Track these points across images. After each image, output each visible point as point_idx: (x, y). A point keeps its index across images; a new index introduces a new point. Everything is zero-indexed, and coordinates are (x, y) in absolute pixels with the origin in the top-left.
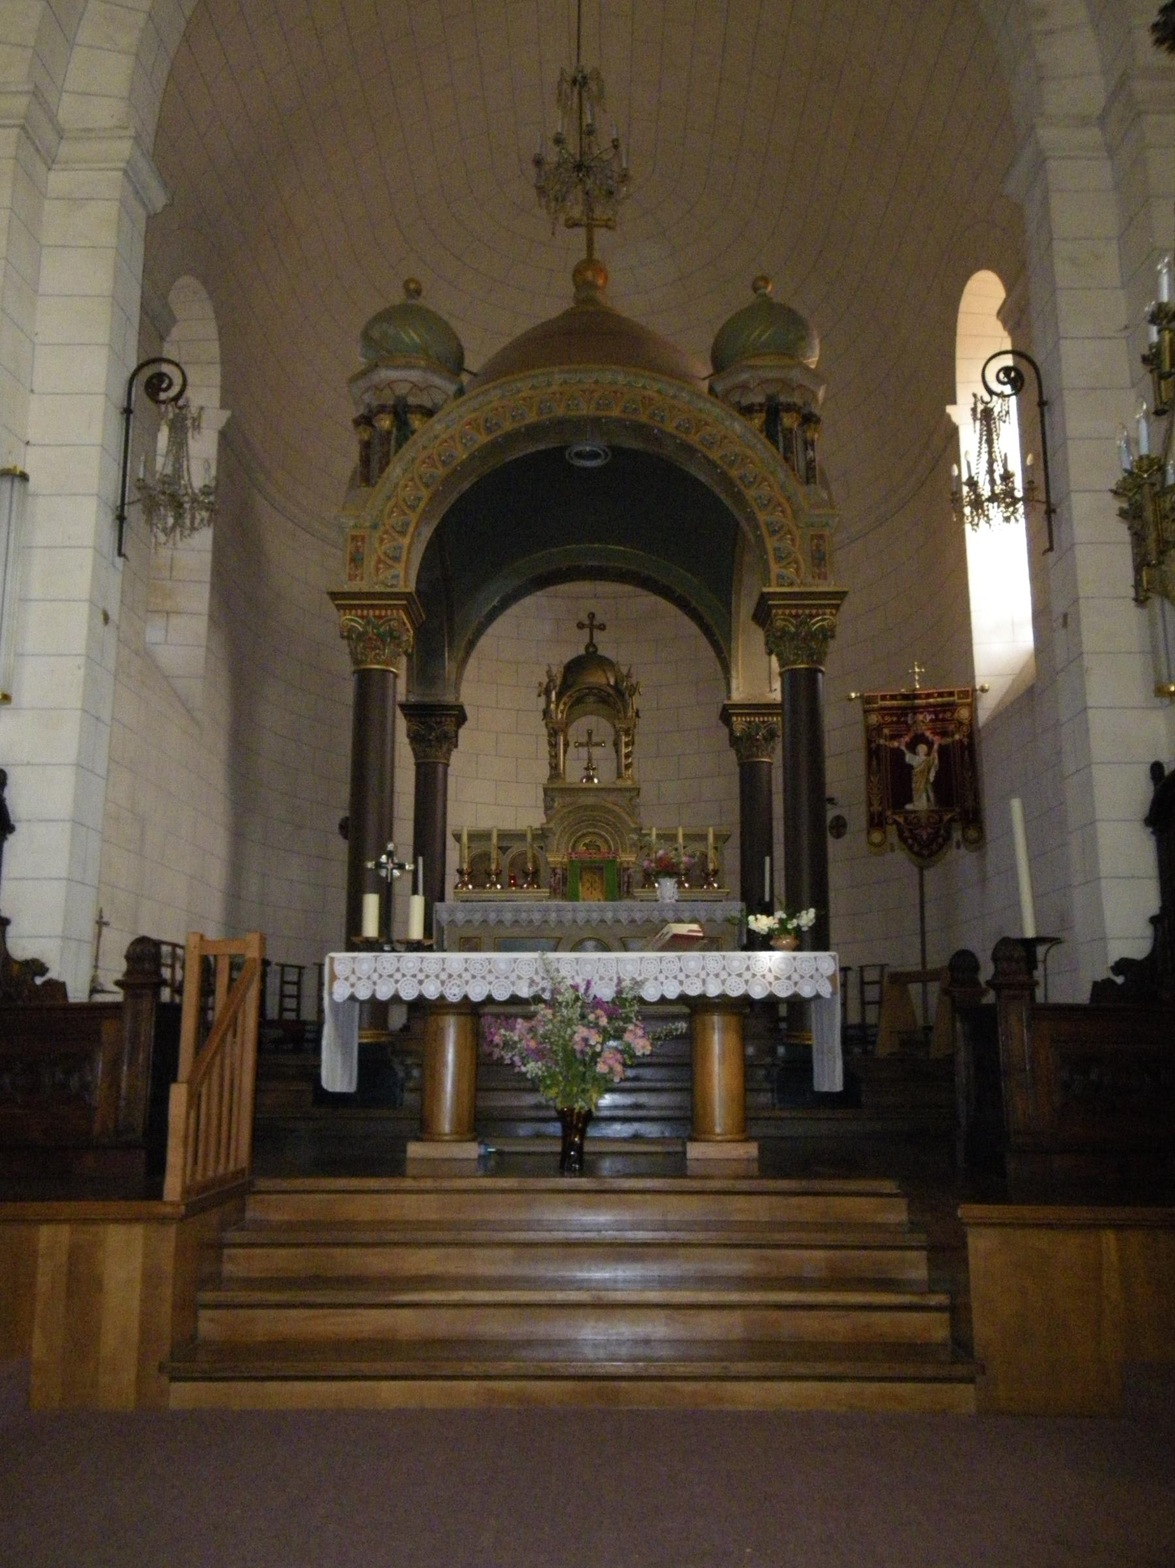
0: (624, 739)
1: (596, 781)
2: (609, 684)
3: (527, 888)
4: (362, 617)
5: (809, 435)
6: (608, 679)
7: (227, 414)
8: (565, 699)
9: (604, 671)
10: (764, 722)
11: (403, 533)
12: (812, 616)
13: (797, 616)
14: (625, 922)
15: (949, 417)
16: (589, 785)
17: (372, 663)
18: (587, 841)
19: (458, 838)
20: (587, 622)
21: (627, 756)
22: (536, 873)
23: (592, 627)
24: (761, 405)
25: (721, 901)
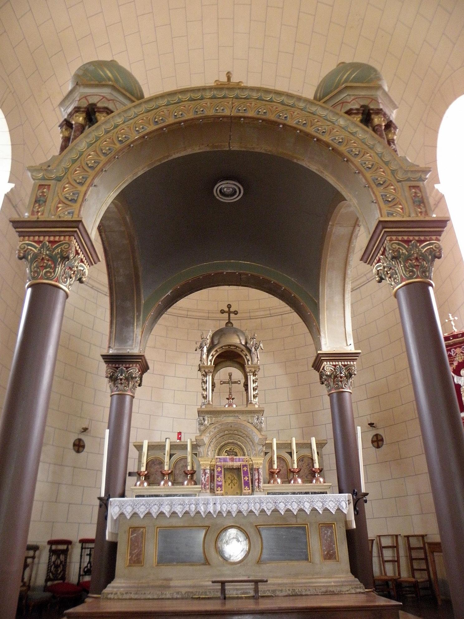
0: (252, 378)
1: (234, 406)
2: (241, 343)
3: (188, 485)
4: (38, 242)
5: (390, 136)
6: (240, 340)
7: (12, 185)
8: (213, 352)
9: (238, 335)
10: (345, 365)
11: (81, 184)
12: (421, 242)
13: (408, 242)
14: (257, 513)
15: (437, 190)
16: (230, 409)
17: (42, 278)
18: (228, 449)
19: (139, 447)
20: (226, 309)
21: (254, 389)
22: (193, 473)
23: (229, 313)
24: (357, 109)
25: (326, 493)
